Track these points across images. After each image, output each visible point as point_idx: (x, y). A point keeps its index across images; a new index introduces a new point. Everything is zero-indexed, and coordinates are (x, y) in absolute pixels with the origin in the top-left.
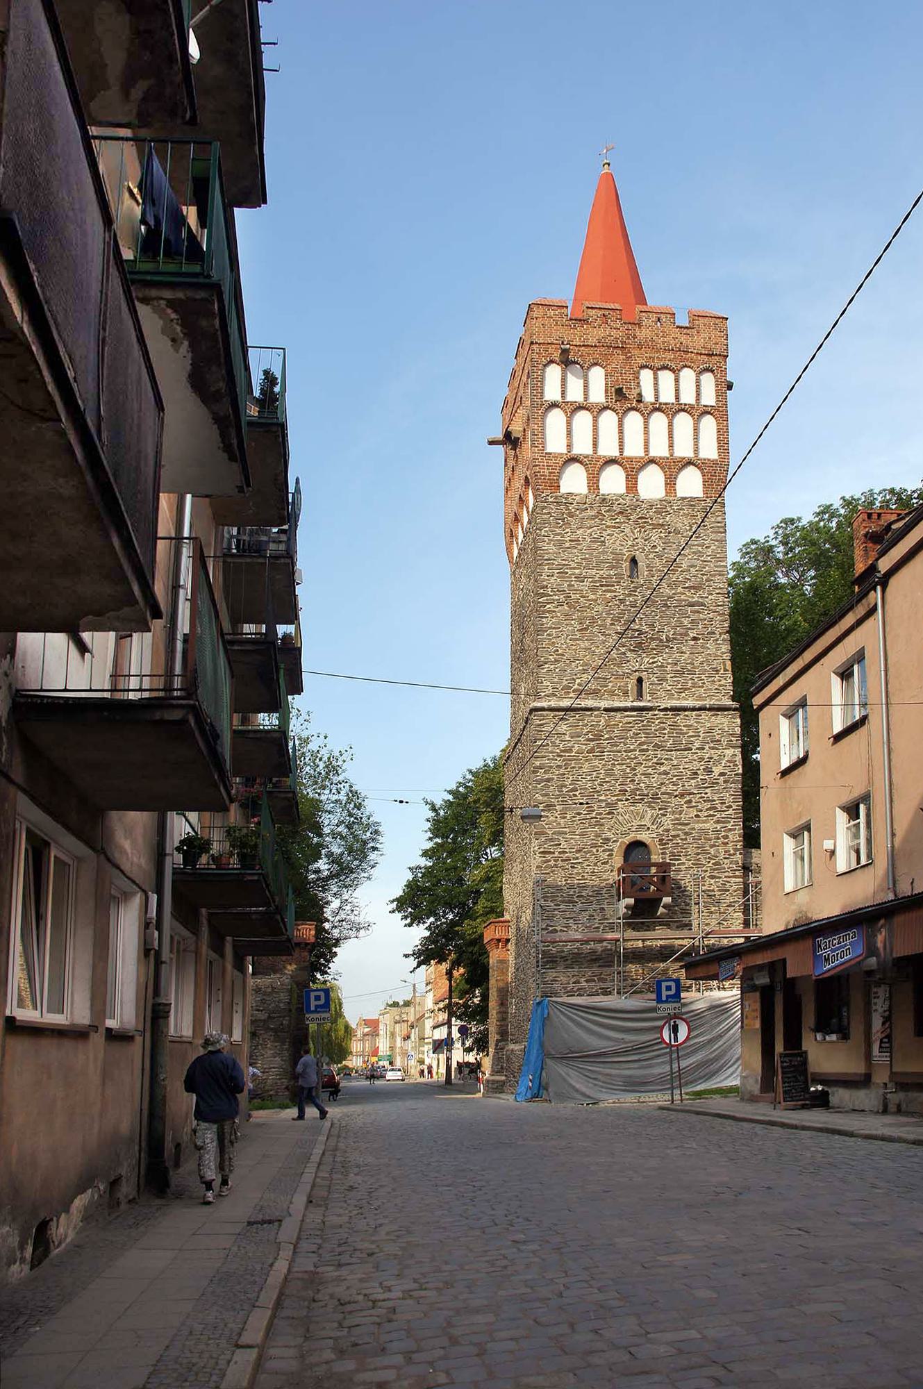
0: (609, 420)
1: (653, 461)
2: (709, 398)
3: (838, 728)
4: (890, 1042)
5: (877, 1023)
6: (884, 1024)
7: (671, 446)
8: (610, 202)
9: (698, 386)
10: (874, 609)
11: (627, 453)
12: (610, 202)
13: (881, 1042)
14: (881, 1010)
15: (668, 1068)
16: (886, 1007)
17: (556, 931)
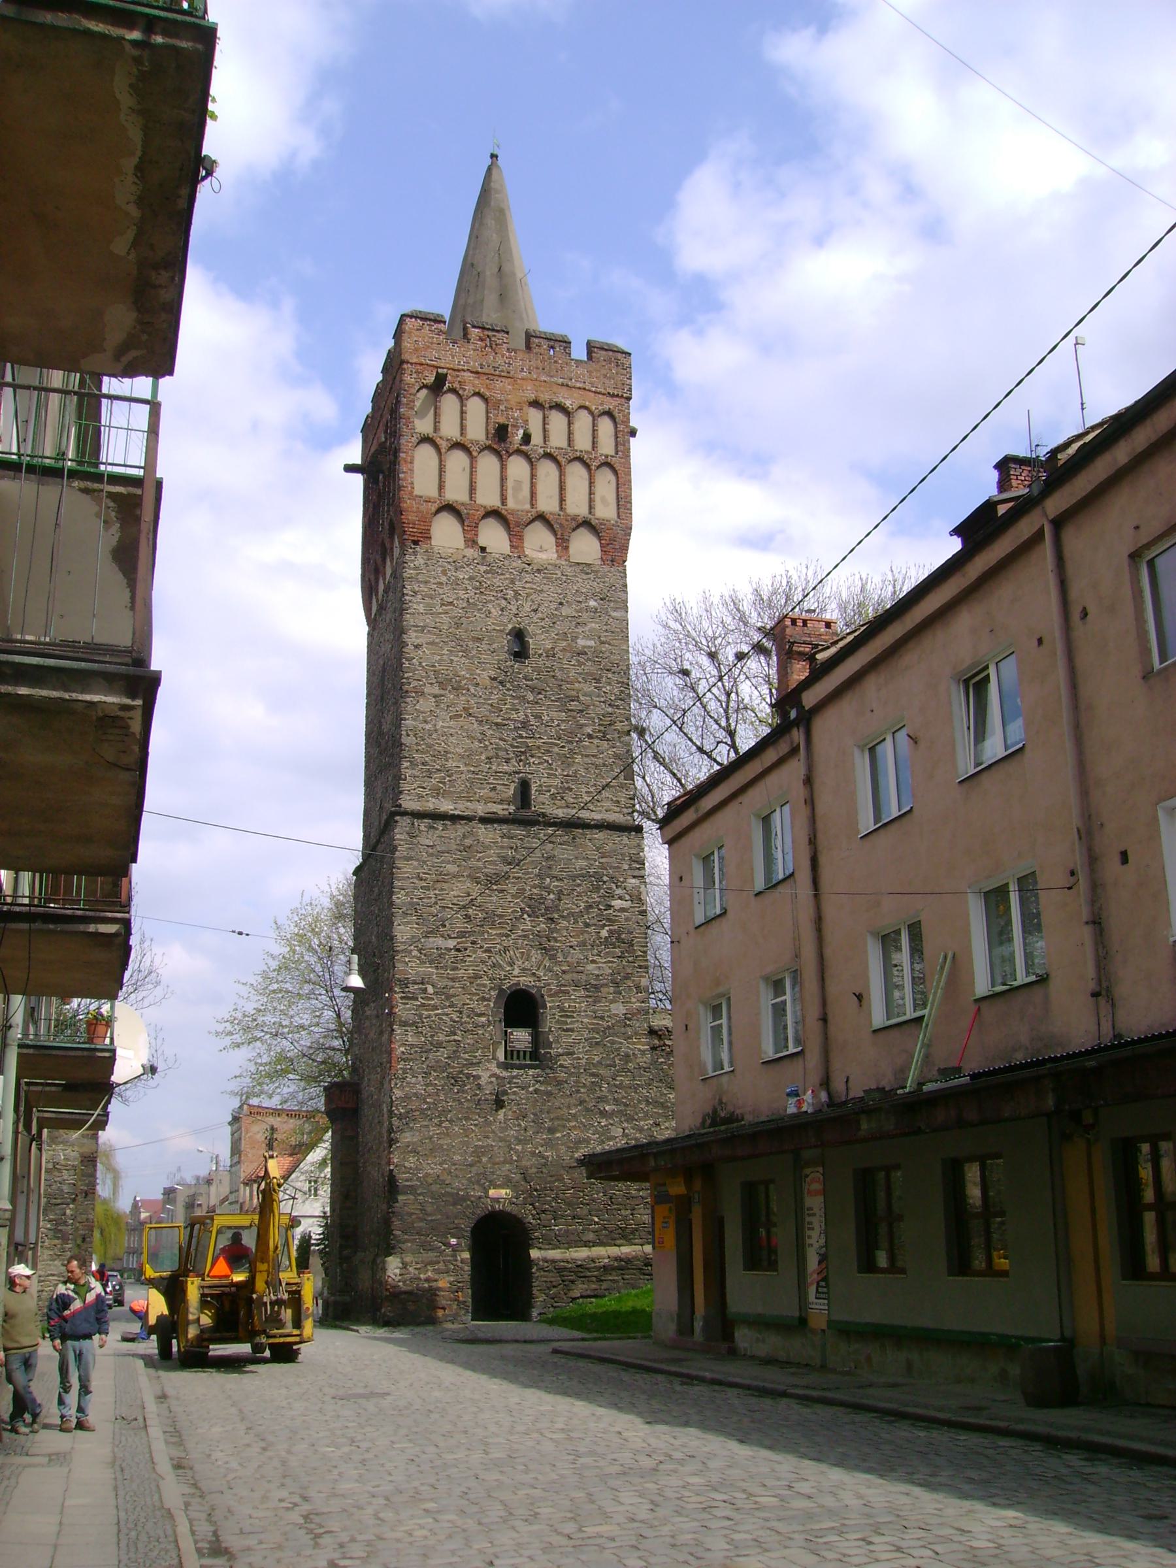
0: (488, 464)
1: (541, 517)
2: (607, 446)
3: (699, 918)
4: (827, 1286)
5: (812, 1263)
6: (820, 1262)
7: (562, 500)
8: (488, 205)
9: (594, 431)
10: (1039, 536)
11: (511, 504)
12: (488, 205)
13: (818, 1283)
14: (816, 1245)
15: (47, 454)
16: (822, 1241)
17: (441, 1164)
